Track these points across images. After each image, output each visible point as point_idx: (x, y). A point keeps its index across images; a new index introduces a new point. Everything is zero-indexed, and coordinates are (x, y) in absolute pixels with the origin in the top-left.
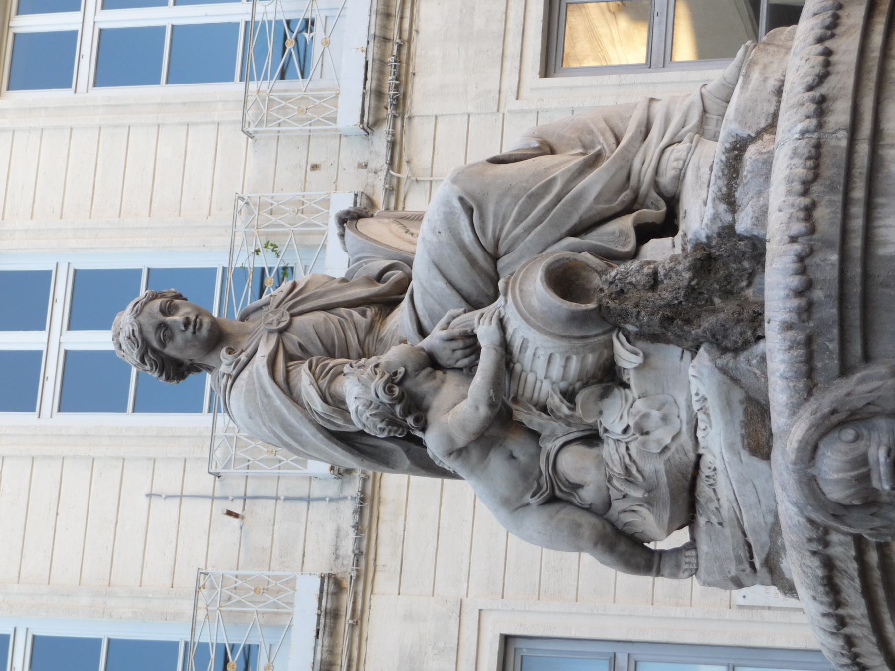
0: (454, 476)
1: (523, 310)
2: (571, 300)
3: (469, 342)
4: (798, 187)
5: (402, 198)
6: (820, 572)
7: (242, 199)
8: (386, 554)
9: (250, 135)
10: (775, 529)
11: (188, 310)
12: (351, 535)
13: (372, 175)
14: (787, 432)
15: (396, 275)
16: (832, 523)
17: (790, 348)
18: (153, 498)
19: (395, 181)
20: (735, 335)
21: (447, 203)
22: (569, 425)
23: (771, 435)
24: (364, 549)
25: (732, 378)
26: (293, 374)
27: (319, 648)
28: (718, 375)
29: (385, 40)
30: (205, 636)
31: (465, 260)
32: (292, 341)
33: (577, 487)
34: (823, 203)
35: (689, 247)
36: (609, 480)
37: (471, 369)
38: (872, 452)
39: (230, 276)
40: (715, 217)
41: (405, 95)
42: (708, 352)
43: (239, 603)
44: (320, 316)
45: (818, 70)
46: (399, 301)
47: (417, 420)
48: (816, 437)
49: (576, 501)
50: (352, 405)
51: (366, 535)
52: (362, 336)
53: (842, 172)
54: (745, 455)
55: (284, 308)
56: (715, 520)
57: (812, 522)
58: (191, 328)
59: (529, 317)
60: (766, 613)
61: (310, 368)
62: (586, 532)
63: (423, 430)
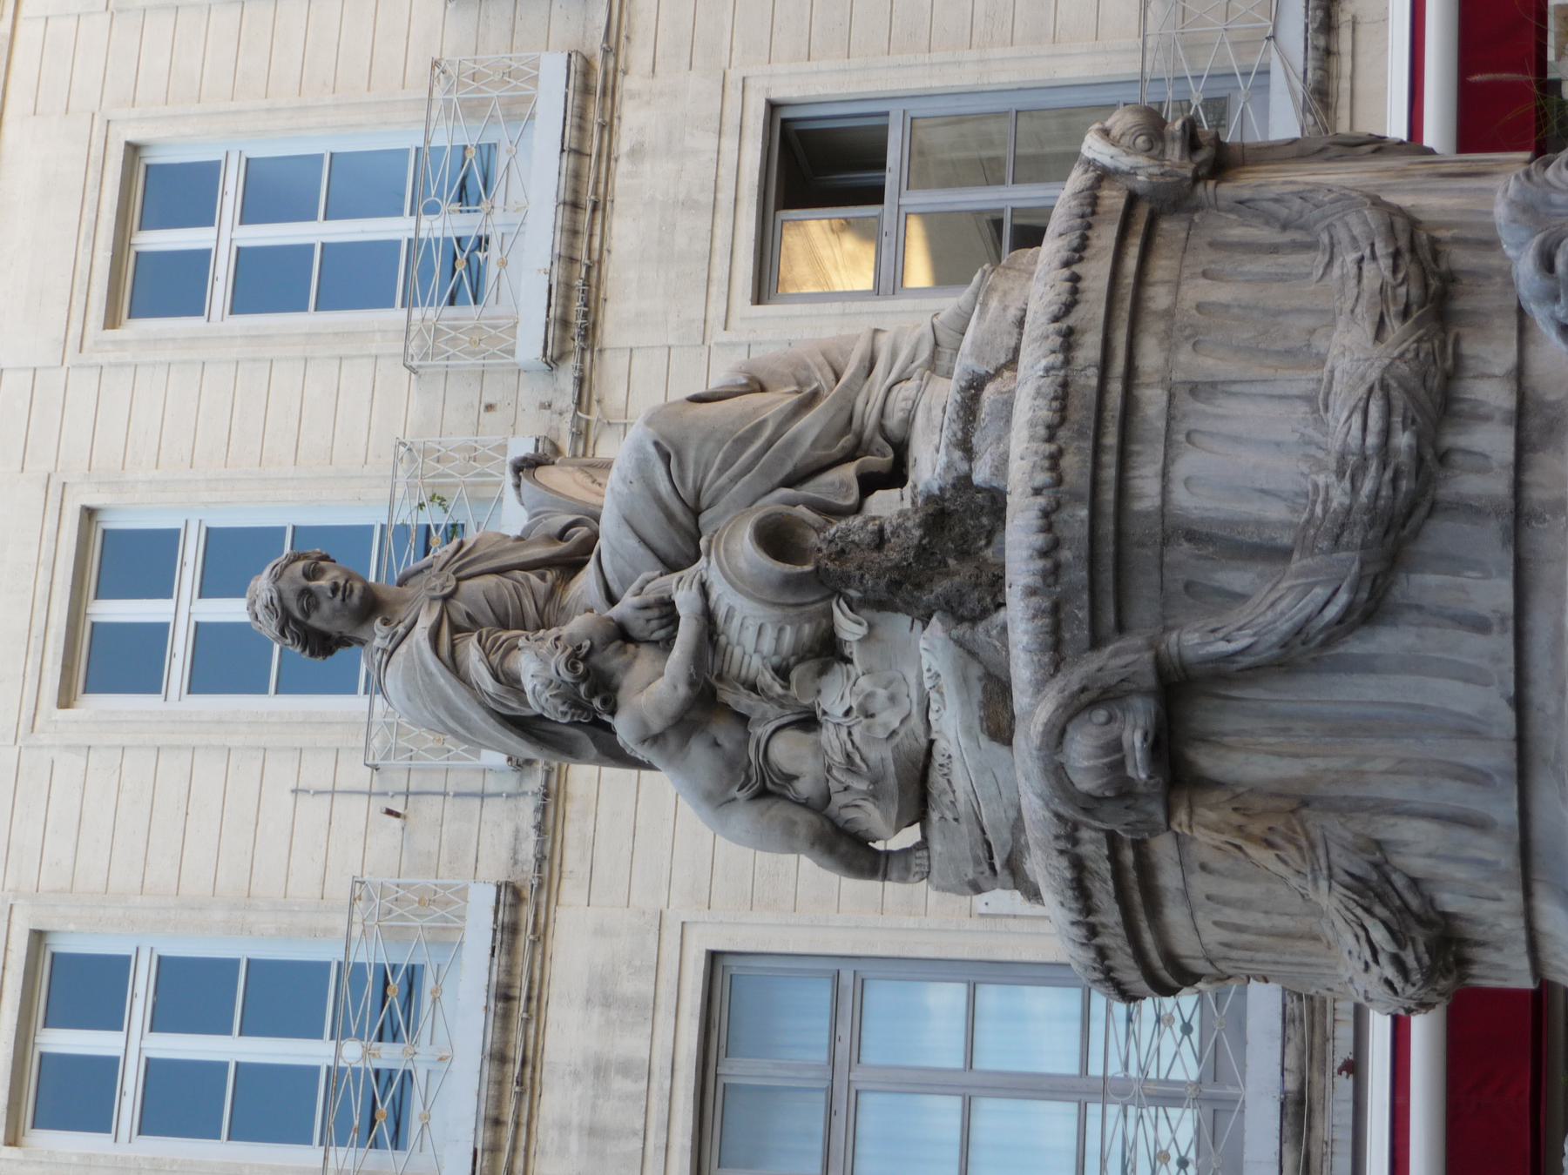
0: (649, 766)
1: (733, 577)
3: (666, 610)
5: (591, 443)
6: (1068, 874)
7: (404, 445)
8: (573, 858)
9: (410, 368)
10: (1018, 826)
13: (556, 416)
14: (1030, 713)
15: (581, 532)
16: (1081, 818)
17: (1034, 617)
18: (300, 795)
19: (583, 424)
21: (639, 448)
22: (782, 706)
23: (1013, 717)
25: (969, 651)
26: (460, 648)
27: (495, 968)
28: (953, 649)
30: (361, 956)
31: (661, 515)
32: (458, 610)
33: (791, 778)
34: (1071, 449)
35: (920, 501)
36: (829, 770)
37: (667, 644)
38: (1126, 736)
39: (389, 534)
40: (950, 466)
44: (491, 580)
45: (1064, 298)
47: (604, 702)
49: (791, 794)
50: (528, 684)
52: (541, 603)
53: (1093, 416)
54: (984, 740)
55: (448, 571)
56: (949, 815)
57: (1058, 816)
58: (340, 594)
59: (736, 581)
60: (1011, 922)
61: (479, 641)
62: (802, 830)
63: (613, 713)
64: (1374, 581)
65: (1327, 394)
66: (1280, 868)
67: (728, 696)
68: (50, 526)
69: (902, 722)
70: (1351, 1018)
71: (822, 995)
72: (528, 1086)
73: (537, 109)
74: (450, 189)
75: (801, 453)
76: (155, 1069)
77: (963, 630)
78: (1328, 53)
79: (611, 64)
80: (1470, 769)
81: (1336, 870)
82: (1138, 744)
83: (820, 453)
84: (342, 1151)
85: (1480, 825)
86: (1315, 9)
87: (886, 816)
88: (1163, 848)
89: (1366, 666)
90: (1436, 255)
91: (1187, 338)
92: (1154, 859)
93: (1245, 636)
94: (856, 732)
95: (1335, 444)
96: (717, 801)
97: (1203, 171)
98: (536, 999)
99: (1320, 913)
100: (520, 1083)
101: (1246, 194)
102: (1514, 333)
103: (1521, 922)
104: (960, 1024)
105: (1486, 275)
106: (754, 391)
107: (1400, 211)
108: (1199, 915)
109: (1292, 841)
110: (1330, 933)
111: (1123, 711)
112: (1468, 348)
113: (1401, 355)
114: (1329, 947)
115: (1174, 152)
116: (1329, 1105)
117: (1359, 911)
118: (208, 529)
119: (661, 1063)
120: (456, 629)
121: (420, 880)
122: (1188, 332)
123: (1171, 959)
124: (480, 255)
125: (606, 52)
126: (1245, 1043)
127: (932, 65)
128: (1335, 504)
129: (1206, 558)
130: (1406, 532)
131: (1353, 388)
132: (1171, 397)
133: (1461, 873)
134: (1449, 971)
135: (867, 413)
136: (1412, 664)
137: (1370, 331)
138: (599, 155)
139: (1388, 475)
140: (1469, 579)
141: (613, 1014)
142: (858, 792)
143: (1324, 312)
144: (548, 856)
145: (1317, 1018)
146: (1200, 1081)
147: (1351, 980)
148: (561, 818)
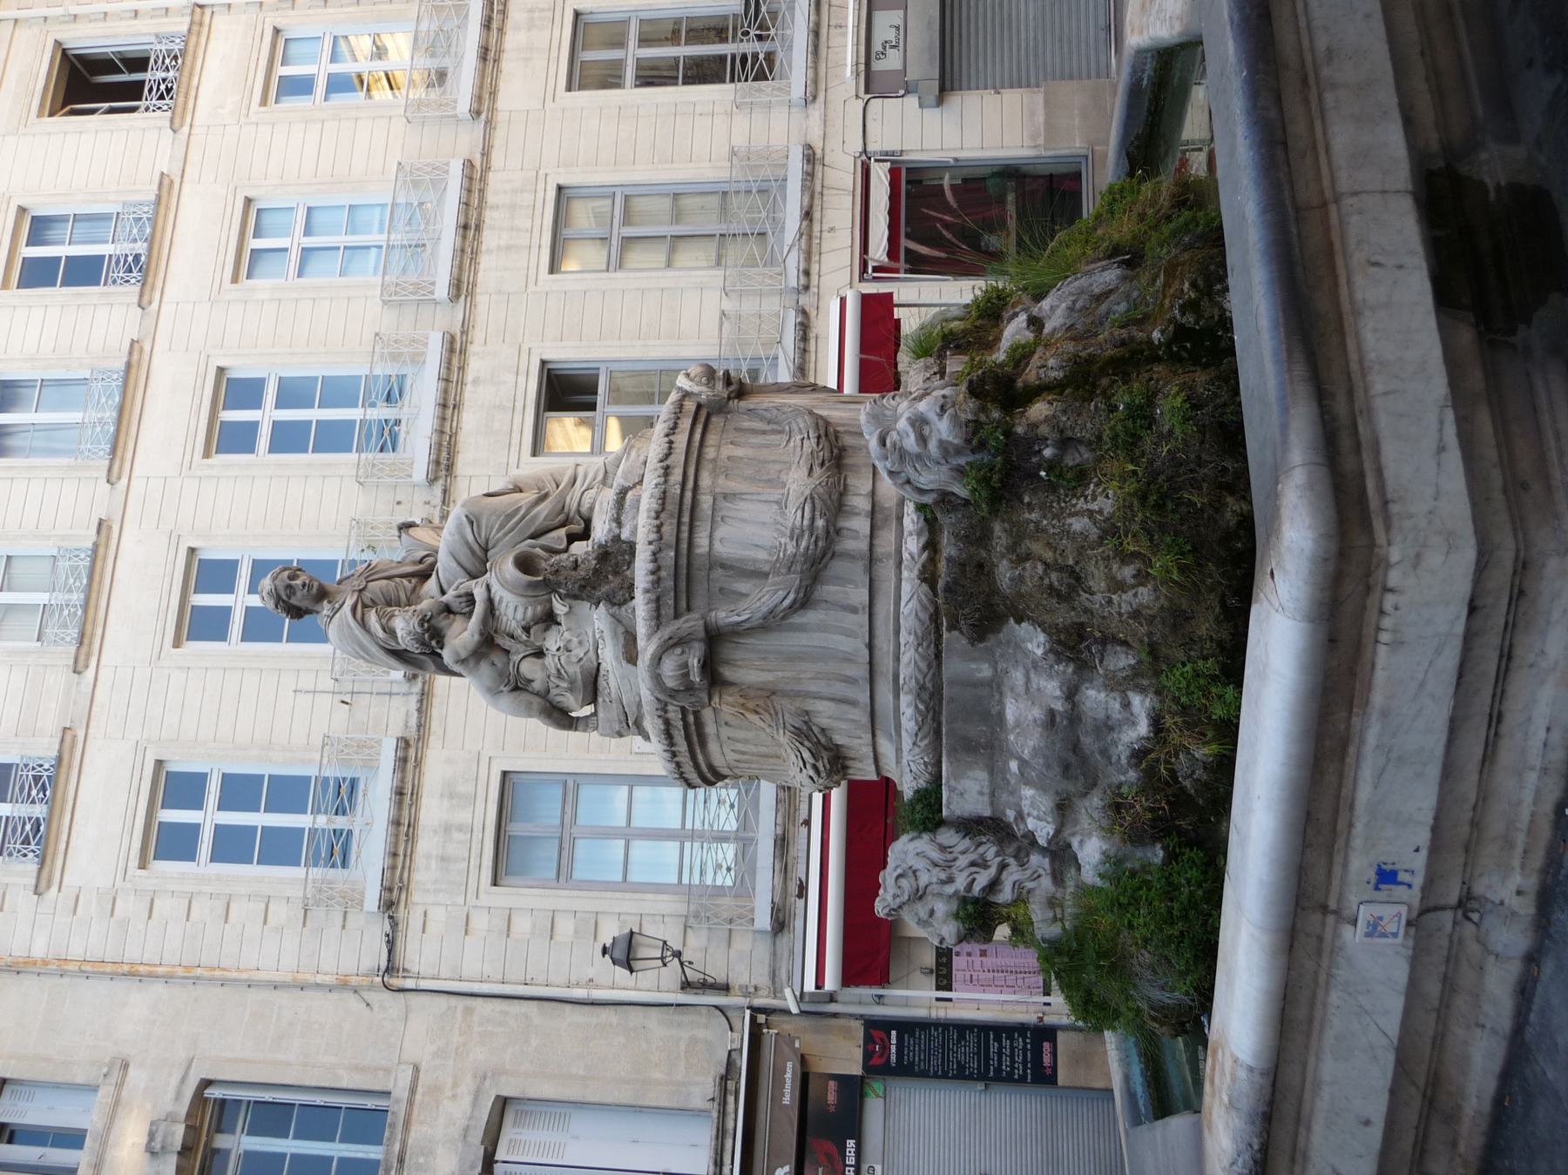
0: (460, 675)
2: (528, 575)
4: (653, 514)
6: (662, 727)
8: (435, 725)
10: (639, 705)
11: (304, 577)
15: (430, 560)
16: (669, 700)
17: (648, 603)
20: (619, 597)
21: (458, 518)
24: (423, 722)
25: (617, 619)
26: (366, 616)
28: (610, 619)
29: (442, 432)
31: (468, 551)
33: (530, 681)
36: (549, 677)
37: (471, 613)
38: (690, 661)
40: (610, 530)
42: (605, 606)
43: (348, 754)
44: (385, 582)
45: (665, 451)
46: (431, 575)
47: (438, 643)
49: (530, 689)
50: (399, 634)
52: (408, 594)
54: (624, 663)
55: (362, 578)
56: (607, 700)
57: (657, 699)
59: (504, 584)
63: (442, 648)
66: (762, 724)
67: (499, 640)
68: (172, 556)
71: (558, 792)
72: (411, 837)
73: (427, 359)
74: (382, 395)
75: (539, 523)
80: (850, 677)
84: (315, 869)
87: (576, 700)
88: (707, 715)
89: (802, 628)
90: (837, 439)
94: (562, 659)
95: (790, 525)
96: (493, 692)
98: (416, 794)
99: (781, 746)
100: (407, 835)
101: (752, 407)
102: (871, 476)
103: (871, 748)
109: (767, 711)
111: (690, 649)
112: (849, 481)
113: (820, 484)
115: (720, 385)
117: (797, 744)
120: (365, 606)
121: (357, 736)
123: (711, 768)
124: (396, 428)
125: (462, 333)
129: (729, 576)
131: (798, 498)
133: (844, 726)
135: (572, 502)
136: (823, 628)
137: (805, 471)
140: (849, 588)
141: (454, 802)
143: (785, 463)
146: (737, 830)
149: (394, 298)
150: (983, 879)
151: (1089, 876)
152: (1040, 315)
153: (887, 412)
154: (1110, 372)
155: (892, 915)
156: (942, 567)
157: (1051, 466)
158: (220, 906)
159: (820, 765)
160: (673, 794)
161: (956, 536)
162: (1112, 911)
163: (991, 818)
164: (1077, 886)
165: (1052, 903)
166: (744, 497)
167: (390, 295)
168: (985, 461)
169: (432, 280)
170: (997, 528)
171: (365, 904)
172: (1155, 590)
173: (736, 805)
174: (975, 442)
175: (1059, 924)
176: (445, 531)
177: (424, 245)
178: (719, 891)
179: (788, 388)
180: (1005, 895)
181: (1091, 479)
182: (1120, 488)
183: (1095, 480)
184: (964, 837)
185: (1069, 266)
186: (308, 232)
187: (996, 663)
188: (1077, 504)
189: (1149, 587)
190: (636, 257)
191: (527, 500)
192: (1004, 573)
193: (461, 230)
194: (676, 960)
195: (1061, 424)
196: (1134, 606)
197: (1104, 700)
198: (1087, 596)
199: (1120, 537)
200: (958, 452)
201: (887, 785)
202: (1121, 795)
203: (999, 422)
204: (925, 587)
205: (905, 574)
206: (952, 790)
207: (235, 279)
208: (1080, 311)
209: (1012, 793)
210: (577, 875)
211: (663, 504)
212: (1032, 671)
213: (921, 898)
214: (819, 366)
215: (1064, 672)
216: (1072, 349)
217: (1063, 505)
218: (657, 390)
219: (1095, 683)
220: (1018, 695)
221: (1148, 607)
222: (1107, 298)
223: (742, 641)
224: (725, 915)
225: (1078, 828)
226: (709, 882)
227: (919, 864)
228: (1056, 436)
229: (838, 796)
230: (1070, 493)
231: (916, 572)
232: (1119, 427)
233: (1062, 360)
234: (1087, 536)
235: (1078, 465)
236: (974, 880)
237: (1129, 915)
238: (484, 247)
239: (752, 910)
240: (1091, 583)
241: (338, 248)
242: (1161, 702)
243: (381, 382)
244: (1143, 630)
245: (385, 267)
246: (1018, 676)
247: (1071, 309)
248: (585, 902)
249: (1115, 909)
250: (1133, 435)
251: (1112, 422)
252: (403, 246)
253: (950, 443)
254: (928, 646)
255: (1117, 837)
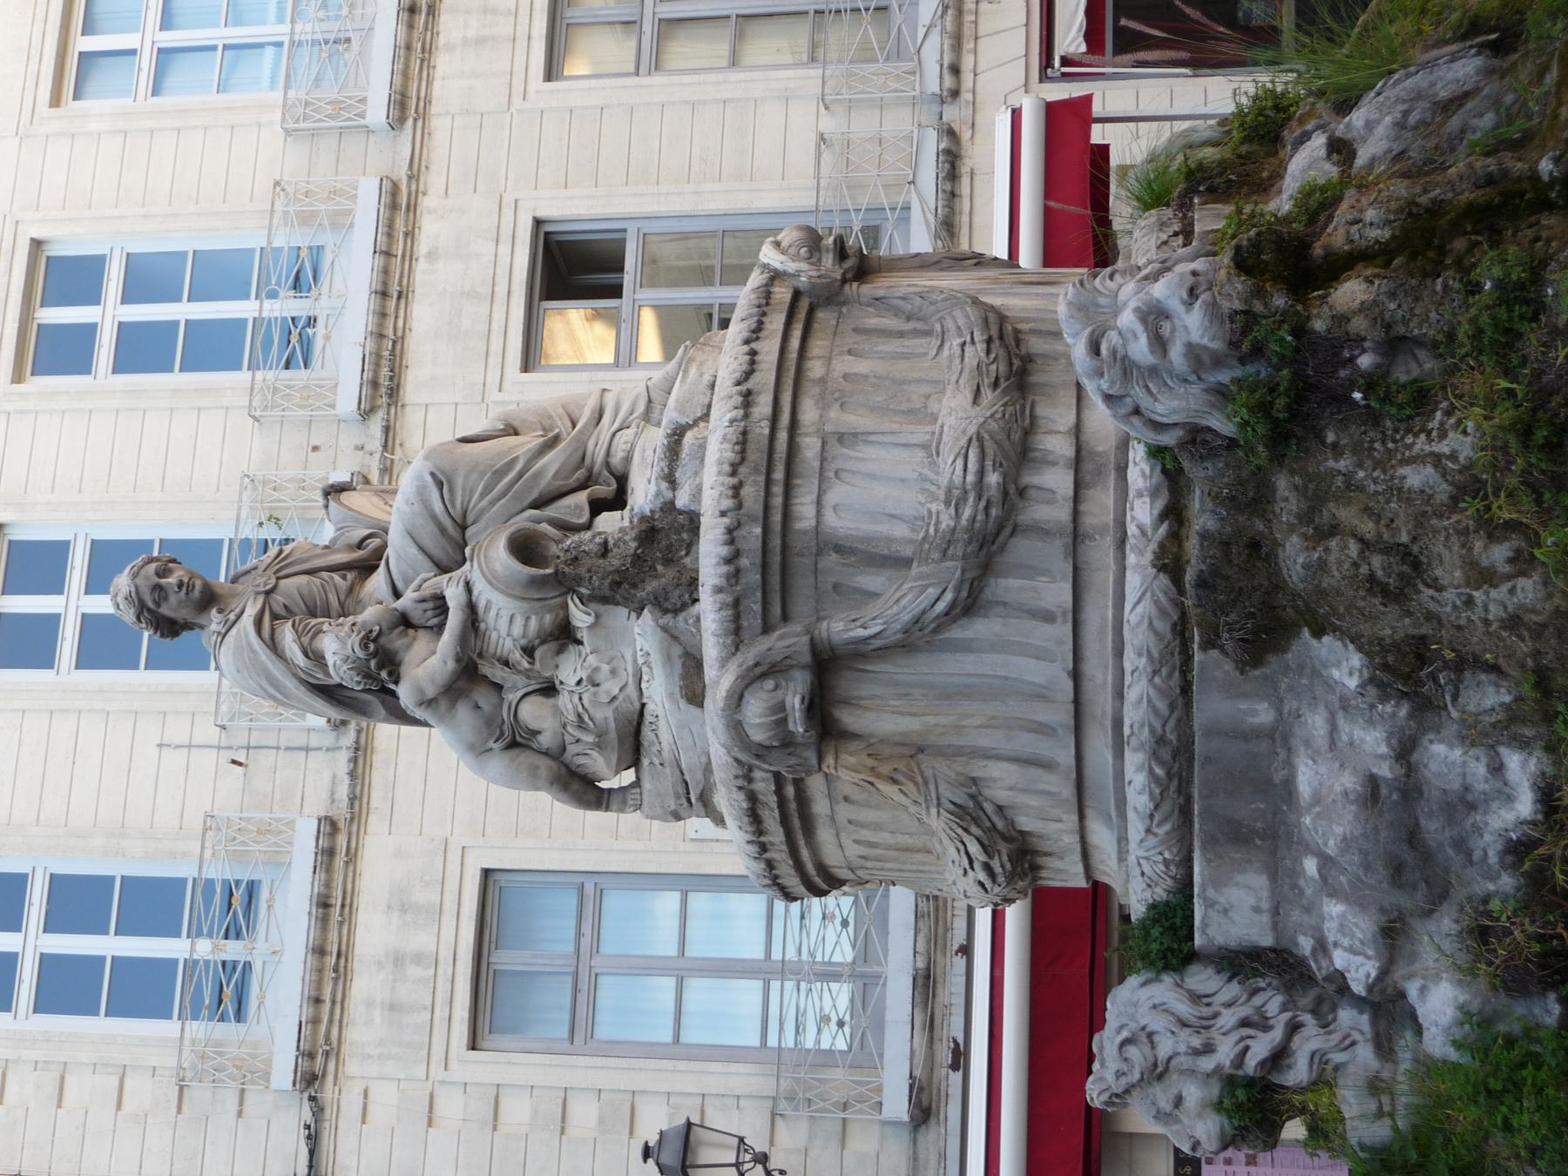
0: (425, 724)
1: (488, 574)
3: (439, 603)
4: (727, 468)
5: (394, 477)
6: (745, 805)
7: (248, 476)
8: (378, 798)
9: (254, 418)
10: (708, 769)
11: (181, 573)
12: (346, 781)
13: (367, 456)
14: (717, 683)
15: (375, 543)
16: (755, 762)
17: (721, 609)
18: (164, 748)
19: (388, 462)
21: (420, 478)
22: (528, 677)
23: (704, 686)
25: (671, 635)
27: (316, 882)
28: (660, 634)
29: (381, 336)
30: (212, 873)
31: (436, 529)
32: (276, 600)
33: (536, 733)
34: (749, 482)
35: (635, 520)
36: (564, 727)
37: (440, 627)
38: (788, 700)
39: (236, 546)
40: (658, 494)
41: (398, 385)
44: (304, 579)
45: (745, 367)
46: (377, 567)
47: (390, 674)
48: (741, 687)
49: (535, 746)
51: (359, 781)
52: (342, 598)
53: (765, 457)
54: (683, 704)
55: (270, 572)
56: (656, 761)
57: (737, 761)
58: (184, 589)
59: (493, 581)
60: (714, 844)
61: (293, 626)
62: (544, 773)
63: (396, 682)
64: (972, 584)
65: (939, 444)
66: (903, 799)
67: (486, 669)
69: (621, 690)
70: (965, 913)
72: (342, 973)
76: (47, 963)
77: (667, 619)
78: (953, 195)
79: (414, 187)
81: (943, 800)
82: (797, 706)
83: (560, 483)
85: (1047, 765)
86: (944, 162)
87: (608, 762)
88: (816, 784)
90: (1018, 342)
91: (836, 400)
92: (809, 793)
93: (876, 625)
95: (944, 482)
96: (478, 750)
97: (849, 275)
98: (348, 905)
99: (933, 833)
101: (881, 293)
103: (1077, 838)
104: (675, 923)
105: (1055, 358)
106: (510, 435)
107: (992, 308)
108: (843, 835)
109: (911, 779)
110: (938, 846)
112: (1041, 411)
113: (992, 415)
114: (938, 858)
115: (828, 260)
116: (948, 978)
117: (960, 831)
118: (93, 541)
119: (445, 954)
120: (275, 617)
122: (836, 395)
123: (822, 869)
124: (310, 331)
125: (410, 178)
126: (888, 933)
127: (660, 194)
128: (943, 526)
129: (849, 565)
130: (995, 548)
131: (957, 439)
132: (824, 443)
133: (1034, 802)
134: (1026, 875)
136: (999, 646)
137: (969, 397)
138: (403, 256)
139: (982, 504)
140: (1041, 583)
142: (588, 743)
144: (358, 795)
145: (940, 914)
146: (854, 962)
147: (954, 883)
148: (368, 765)
149: (302, 125)
150: (1261, 1048)
151: (1437, 1043)
152: (1349, 136)
153: (1102, 301)
154: (1469, 228)
155: (1113, 1104)
156: (1192, 546)
157: (1371, 383)
158: (49, 1079)
159: (996, 865)
160: (750, 906)
161: (1217, 499)
162: (1476, 1102)
163: (1273, 950)
164: (1416, 1060)
165: (1375, 1086)
166: (871, 438)
167: (297, 121)
168: (1263, 375)
169: (361, 94)
170: (1283, 484)
171: (272, 1079)
172: (1545, 584)
173: (851, 921)
174: (1246, 347)
175: (1388, 1121)
176: (399, 497)
177: (348, 40)
178: (826, 1058)
179: (938, 262)
180: (1298, 1073)
181: (1437, 403)
182: (1486, 418)
183: (1444, 405)
184: (1230, 979)
185: (1394, 53)
186: (166, 23)
187: (1281, 700)
188: (1414, 443)
189: (1536, 577)
190: (682, 50)
191: (530, 445)
192: (1294, 556)
193: (406, 14)
194: (759, 1167)
195: (1387, 316)
196: (1510, 609)
197: (1459, 760)
198: (1431, 592)
199: (1485, 497)
200: (1218, 362)
201: (1098, 893)
202: (1489, 915)
203: (1285, 313)
204: (1164, 580)
205: (1132, 559)
206: (1210, 904)
207: (56, 101)
208: (1416, 128)
209: (1308, 910)
210: (604, 1031)
211: (743, 451)
212: (1340, 714)
213: (1160, 1077)
214: (976, 219)
215: (1394, 715)
216: (1404, 193)
217: (1390, 445)
218: (716, 263)
219: (1444, 733)
220: (1317, 752)
221: (1533, 611)
222: (1461, 105)
223: (869, 668)
224: (836, 1096)
225: (1417, 966)
226: (809, 1044)
227: (1158, 1023)
228: (1378, 334)
229: (1016, 917)
230: (1403, 426)
231: (1149, 556)
232: (1485, 319)
233: (1388, 211)
234: (1430, 497)
235: (1415, 381)
236: (1247, 1049)
237: (1504, 1109)
238: (441, 41)
239: (879, 1090)
240: (1438, 572)
241: (214, 48)
242: (1554, 763)
243: (284, 260)
244: (1524, 648)
245: (288, 76)
246: (1316, 723)
247: (1400, 125)
248: (615, 1075)
249: (1481, 1099)
250: (1508, 331)
251: (1473, 311)
252: (315, 42)
253: (1205, 348)
254: (1170, 675)
255: (1482, 983)
